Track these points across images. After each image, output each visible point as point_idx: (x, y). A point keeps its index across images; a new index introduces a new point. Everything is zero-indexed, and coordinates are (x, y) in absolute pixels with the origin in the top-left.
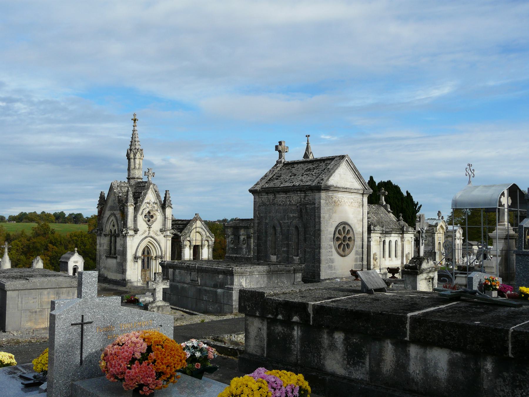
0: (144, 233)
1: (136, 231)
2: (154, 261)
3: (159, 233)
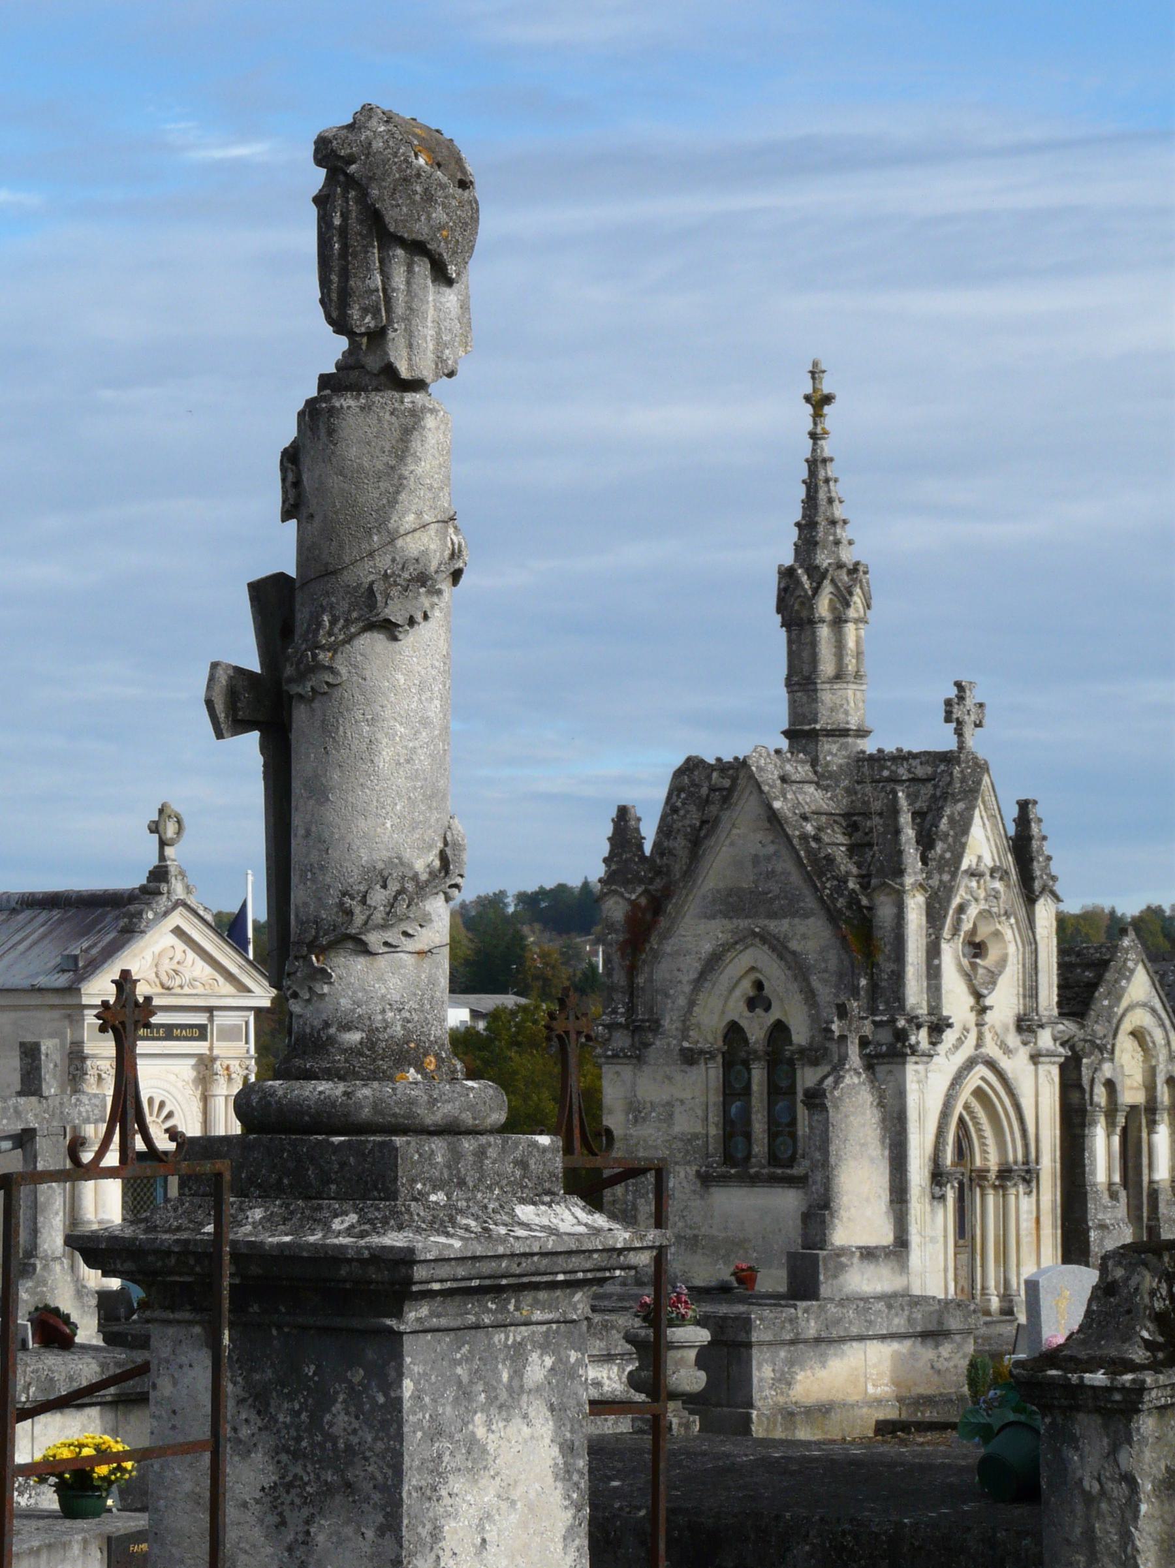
2: (991, 1199)
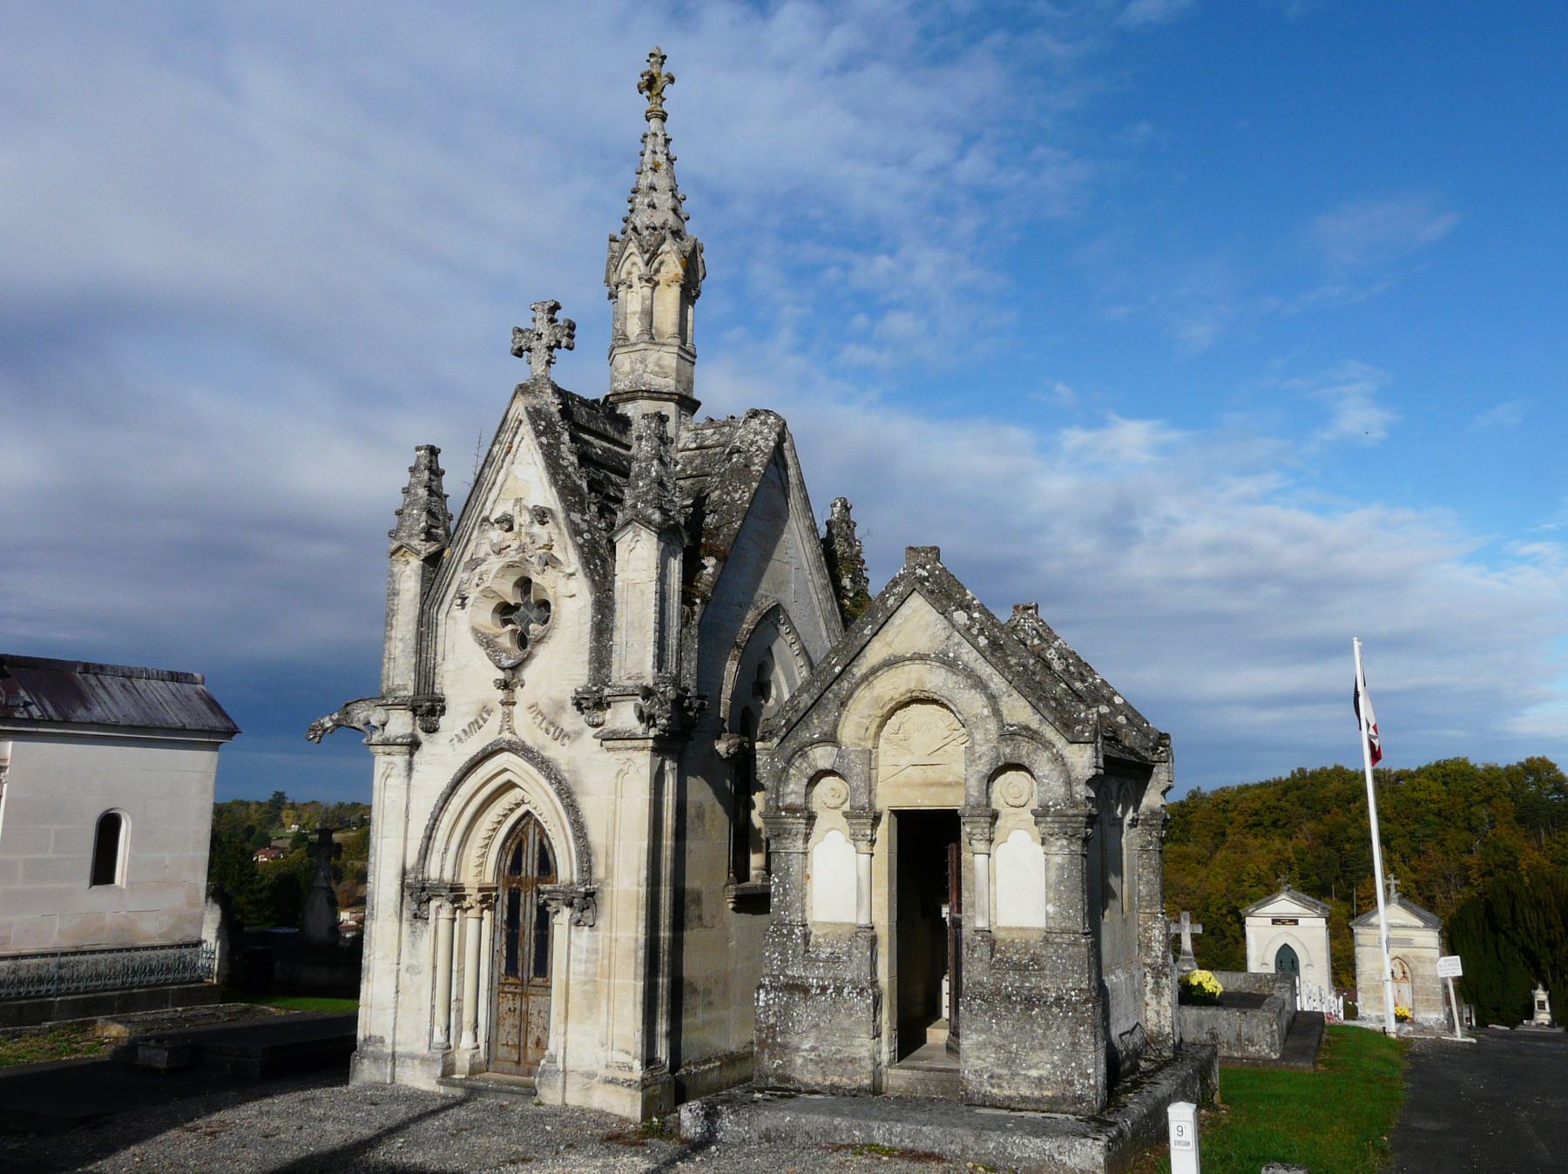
0: (476, 725)
1: (428, 708)
3: (572, 720)
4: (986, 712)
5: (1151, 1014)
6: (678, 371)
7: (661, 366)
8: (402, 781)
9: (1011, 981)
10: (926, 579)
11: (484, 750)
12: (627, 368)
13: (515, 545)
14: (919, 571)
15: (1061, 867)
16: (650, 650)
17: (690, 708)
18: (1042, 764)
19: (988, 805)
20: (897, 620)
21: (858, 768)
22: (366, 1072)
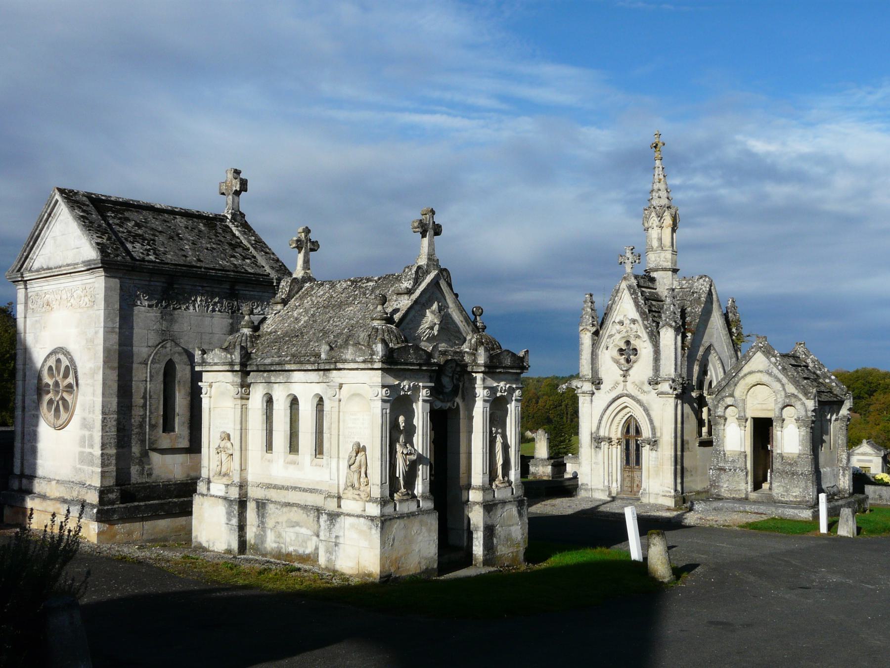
0: (614, 388)
1: (597, 382)
3: (647, 387)
4: (781, 389)
5: (841, 482)
6: (672, 260)
7: (666, 259)
8: (589, 405)
9: (788, 468)
10: (762, 347)
11: (618, 396)
12: (653, 259)
13: (625, 331)
14: (760, 345)
15: (804, 436)
16: (673, 366)
17: (685, 383)
18: (798, 405)
19: (781, 417)
20: (753, 360)
21: (741, 405)
22: (582, 494)
